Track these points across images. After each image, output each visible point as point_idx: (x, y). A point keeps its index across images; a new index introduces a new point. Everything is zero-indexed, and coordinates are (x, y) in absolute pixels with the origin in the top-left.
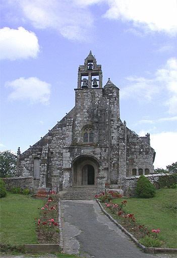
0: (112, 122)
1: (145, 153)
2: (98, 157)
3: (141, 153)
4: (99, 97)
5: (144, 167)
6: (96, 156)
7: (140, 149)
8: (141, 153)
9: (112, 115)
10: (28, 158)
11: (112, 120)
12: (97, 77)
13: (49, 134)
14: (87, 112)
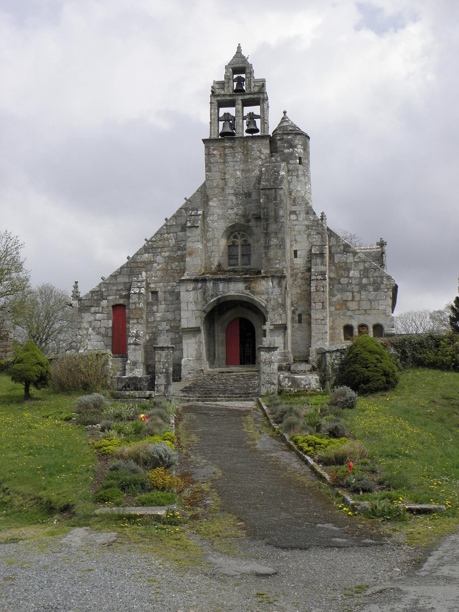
0: (293, 217)
1: (371, 288)
4: (263, 157)
6: (256, 298)
7: (361, 279)
8: (363, 287)
9: (294, 201)
10: (98, 305)
11: (294, 213)
12: (256, 110)
13: (146, 249)
14: (236, 195)
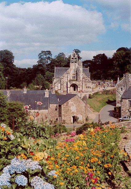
2: (77, 84)
3: (88, 82)
5: (89, 86)
8: (88, 82)
